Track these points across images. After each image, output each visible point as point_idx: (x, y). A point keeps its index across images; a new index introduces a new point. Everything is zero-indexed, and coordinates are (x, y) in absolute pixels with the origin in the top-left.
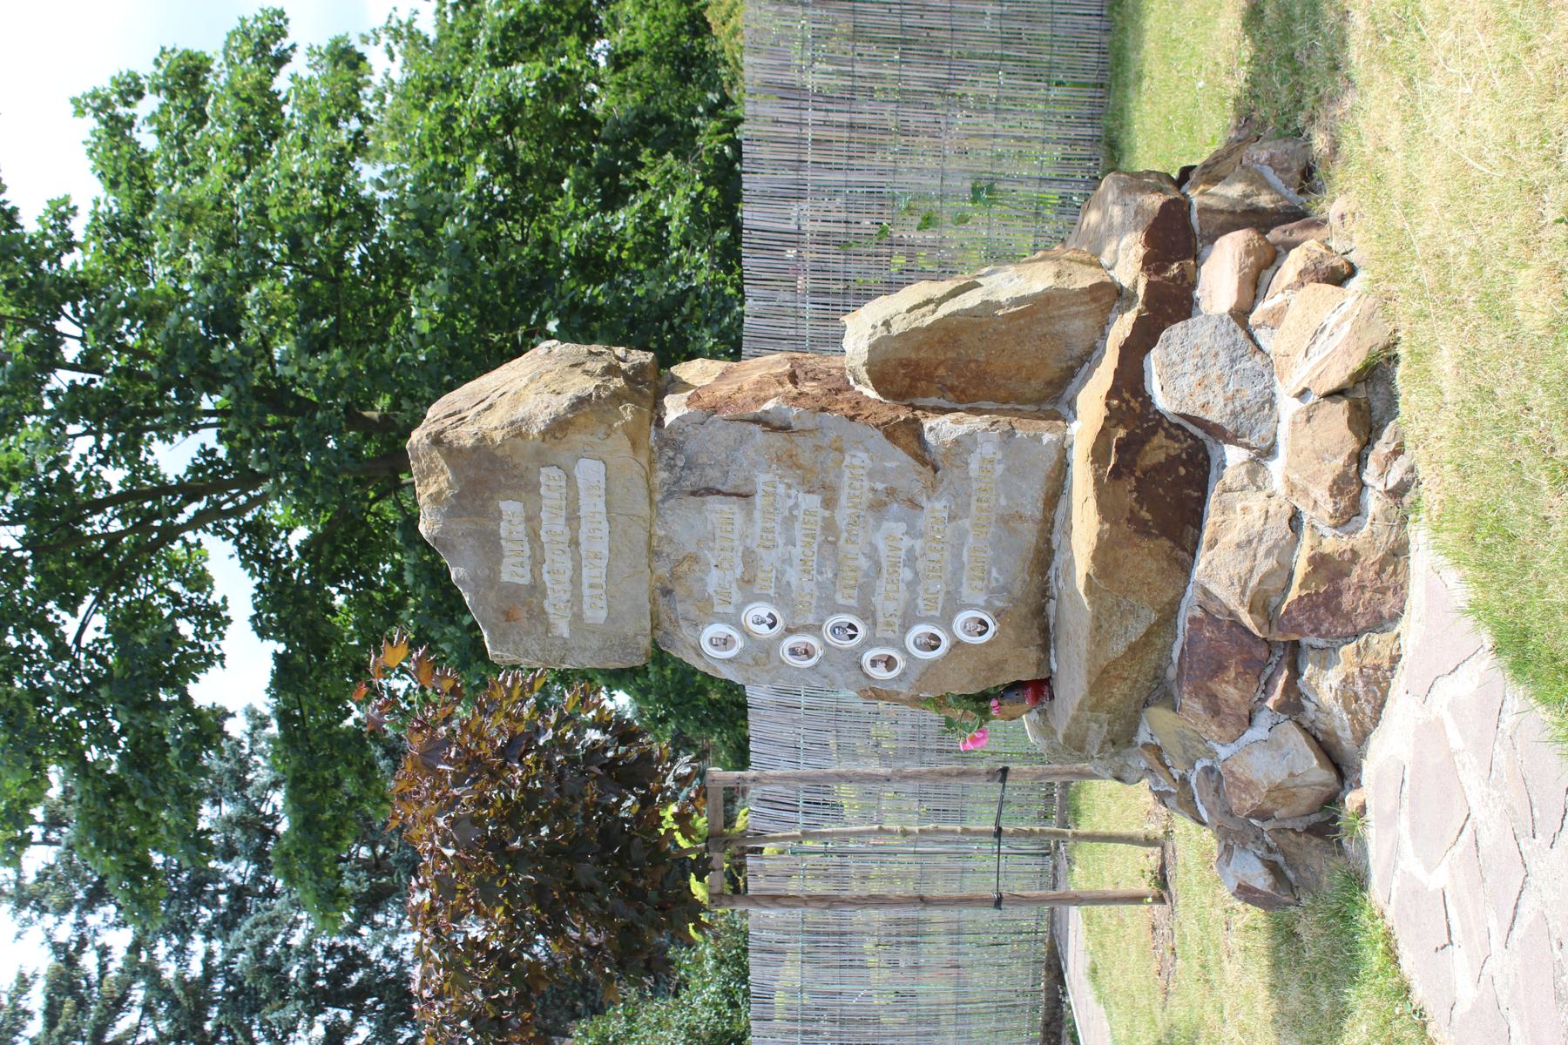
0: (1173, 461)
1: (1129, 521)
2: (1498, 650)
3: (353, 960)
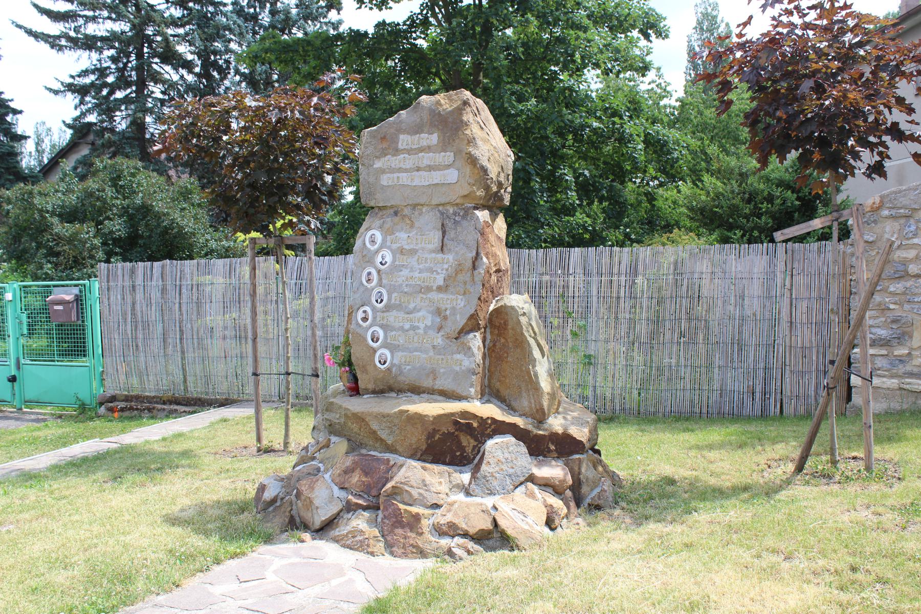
0: (462, 449)
1: (434, 429)
2: (377, 600)
3: (224, 73)
